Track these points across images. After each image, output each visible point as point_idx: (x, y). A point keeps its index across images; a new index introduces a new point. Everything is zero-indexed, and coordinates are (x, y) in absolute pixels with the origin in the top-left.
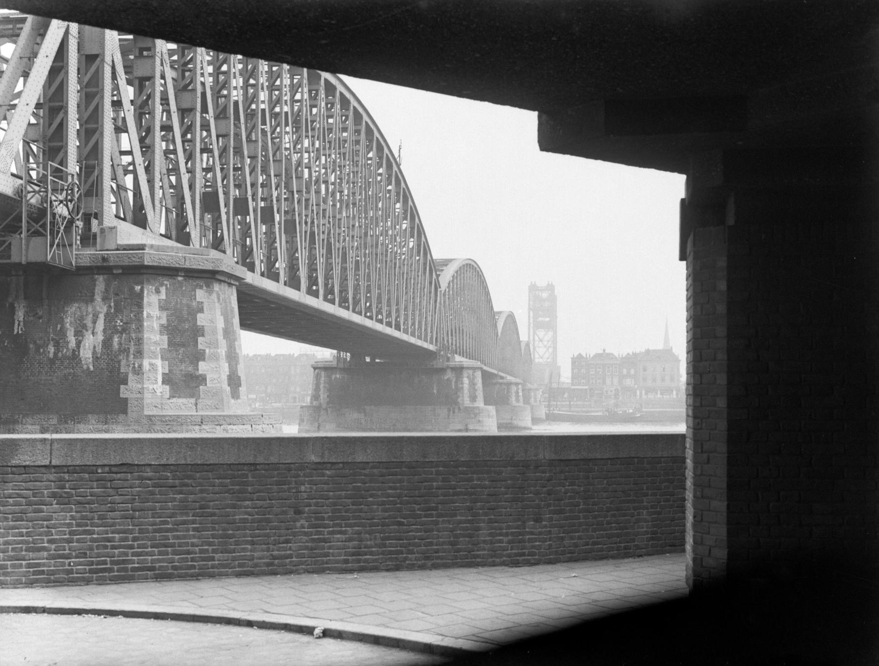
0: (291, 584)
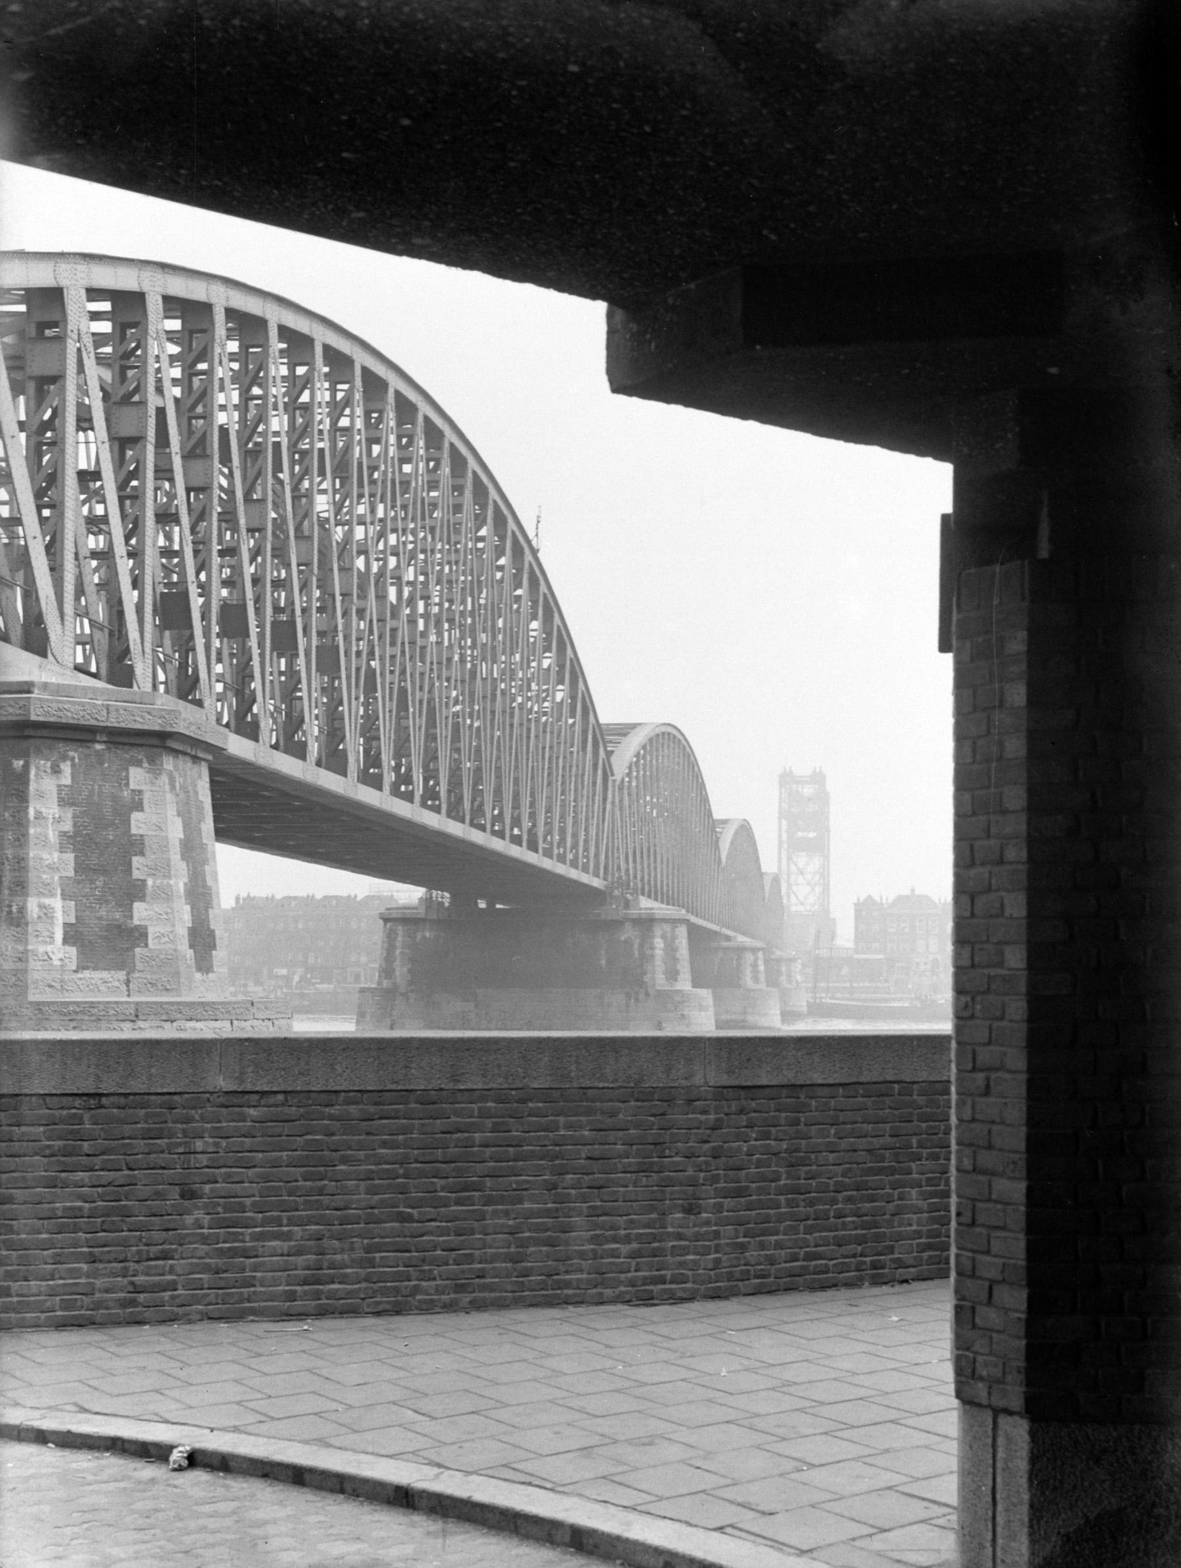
0: (167, 1346)
